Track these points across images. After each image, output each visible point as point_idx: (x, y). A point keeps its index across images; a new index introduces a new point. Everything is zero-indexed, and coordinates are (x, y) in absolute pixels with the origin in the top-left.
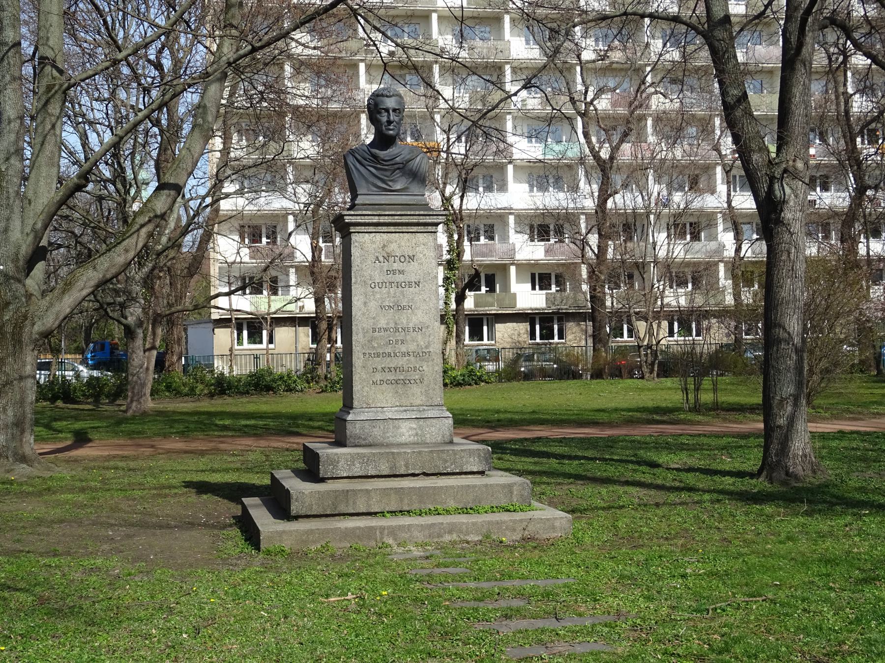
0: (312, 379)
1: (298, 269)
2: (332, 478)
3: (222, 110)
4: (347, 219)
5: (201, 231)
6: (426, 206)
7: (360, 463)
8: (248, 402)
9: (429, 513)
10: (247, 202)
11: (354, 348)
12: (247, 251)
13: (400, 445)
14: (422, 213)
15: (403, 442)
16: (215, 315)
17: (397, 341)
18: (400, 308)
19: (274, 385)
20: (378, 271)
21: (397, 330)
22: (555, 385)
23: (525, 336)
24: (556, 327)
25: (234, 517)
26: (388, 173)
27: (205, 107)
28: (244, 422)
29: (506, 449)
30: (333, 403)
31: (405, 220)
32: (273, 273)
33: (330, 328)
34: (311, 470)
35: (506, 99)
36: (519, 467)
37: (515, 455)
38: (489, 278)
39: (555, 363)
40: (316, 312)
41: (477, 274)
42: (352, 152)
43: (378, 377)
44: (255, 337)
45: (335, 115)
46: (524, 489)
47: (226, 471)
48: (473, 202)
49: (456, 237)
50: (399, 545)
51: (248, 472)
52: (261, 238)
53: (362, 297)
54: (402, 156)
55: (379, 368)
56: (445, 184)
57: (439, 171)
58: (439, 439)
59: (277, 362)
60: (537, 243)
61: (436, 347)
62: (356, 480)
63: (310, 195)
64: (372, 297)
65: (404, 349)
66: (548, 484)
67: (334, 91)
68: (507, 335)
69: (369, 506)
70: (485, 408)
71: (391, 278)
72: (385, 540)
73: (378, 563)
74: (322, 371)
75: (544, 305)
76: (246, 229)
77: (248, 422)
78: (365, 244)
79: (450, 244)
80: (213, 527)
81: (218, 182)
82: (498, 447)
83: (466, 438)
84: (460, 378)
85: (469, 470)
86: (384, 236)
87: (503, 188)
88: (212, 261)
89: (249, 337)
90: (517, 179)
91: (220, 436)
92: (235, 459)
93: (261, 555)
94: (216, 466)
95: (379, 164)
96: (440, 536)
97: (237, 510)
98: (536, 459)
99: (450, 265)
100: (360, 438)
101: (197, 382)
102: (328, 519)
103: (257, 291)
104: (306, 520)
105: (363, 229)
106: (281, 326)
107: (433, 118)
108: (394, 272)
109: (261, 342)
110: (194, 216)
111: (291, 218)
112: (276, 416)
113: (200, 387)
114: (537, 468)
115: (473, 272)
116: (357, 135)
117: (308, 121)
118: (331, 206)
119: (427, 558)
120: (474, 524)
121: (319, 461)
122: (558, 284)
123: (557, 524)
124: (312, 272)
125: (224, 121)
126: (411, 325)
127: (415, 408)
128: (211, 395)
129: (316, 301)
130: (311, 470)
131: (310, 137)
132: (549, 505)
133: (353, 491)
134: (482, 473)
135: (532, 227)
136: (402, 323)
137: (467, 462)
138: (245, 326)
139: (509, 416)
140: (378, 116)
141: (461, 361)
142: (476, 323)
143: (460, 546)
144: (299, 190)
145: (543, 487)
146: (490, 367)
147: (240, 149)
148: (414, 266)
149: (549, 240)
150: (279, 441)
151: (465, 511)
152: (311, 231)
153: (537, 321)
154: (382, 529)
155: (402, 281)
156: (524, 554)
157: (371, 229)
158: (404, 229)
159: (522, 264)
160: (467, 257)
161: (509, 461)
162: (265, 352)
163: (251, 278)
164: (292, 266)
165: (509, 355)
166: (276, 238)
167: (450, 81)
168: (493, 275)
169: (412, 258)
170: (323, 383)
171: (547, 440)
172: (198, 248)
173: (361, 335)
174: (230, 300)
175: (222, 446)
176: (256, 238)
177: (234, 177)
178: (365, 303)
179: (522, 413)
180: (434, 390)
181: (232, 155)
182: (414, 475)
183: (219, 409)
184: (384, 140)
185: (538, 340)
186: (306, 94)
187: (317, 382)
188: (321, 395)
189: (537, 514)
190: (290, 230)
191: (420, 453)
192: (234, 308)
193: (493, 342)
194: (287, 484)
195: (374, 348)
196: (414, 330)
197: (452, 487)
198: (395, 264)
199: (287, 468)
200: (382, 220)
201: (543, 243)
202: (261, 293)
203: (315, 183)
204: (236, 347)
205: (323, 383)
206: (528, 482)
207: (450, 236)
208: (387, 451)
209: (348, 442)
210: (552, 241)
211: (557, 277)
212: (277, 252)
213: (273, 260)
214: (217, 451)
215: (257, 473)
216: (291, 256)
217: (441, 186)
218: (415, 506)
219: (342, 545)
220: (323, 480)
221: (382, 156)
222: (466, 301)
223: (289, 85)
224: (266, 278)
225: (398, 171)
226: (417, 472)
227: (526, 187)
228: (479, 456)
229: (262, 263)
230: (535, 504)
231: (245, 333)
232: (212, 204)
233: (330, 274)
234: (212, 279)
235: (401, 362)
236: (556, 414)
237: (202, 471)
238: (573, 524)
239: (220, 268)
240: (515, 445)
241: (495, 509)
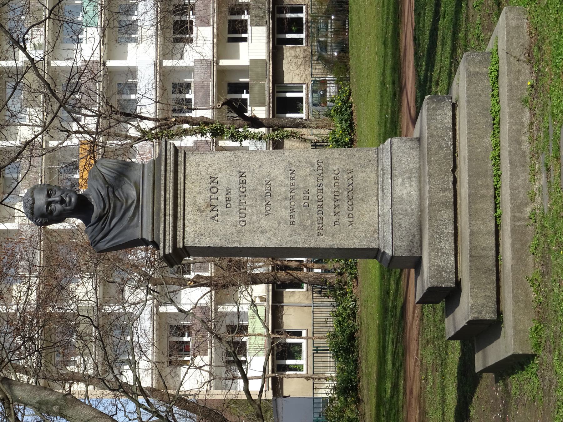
0: (342, 289)
1: (218, 302)
2: (456, 273)
3: (42, 382)
4: (169, 250)
5: (175, 409)
6: (156, 163)
7: (440, 242)
8: (367, 360)
9: (497, 166)
10: (144, 358)
11: (311, 246)
12: (198, 358)
13: (421, 197)
14: (163, 167)
15: (417, 193)
16: (269, 395)
17: (305, 198)
18: (268, 194)
19: (348, 331)
21: (293, 198)
22: (355, 18)
23: (298, 50)
24: (289, 15)
25: (497, 382)
26: (119, 204)
27: (40, 403)
28: (389, 366)
29: (426, 76)
30: (370, 269)
31: (170, 187)
32: (223, 330)
33: (285, 268)
34: (446, 296)
35: (36, 69)
36: (447, 62)
37: (433, 66)
38: (232, 89)
39: (330, 18)
40: (268, 283)
41: (228, 103)
42: (94, 243)
43: (344, 220)
44: (293, 351)
45: (48, 258)
46: (473, 60)
47: (443, 388)
48: (147, 106)
49: (186, 126)
50: (533, 200)
51: (446, 364)
52: (184, 343)
53: (255, 236)
54: (100, 188)
55: (334, 218)
56: (127, 137)
57: (112, 143)
58: (415, 153)
59: (322, 327)
60: (194, 36)
61: (314, 155)
62: (459, 246)
63: (137, 287)
64: (256, 225)
65: (314, 191)
66: (467, 31)
67: (22, 258)
68: (297, 71)
69: (488, 233)
70: (378, 98)
72: (526, 216)
73: (553, 225)
74: (333, 278)
75: (264, 28)
76: (174, 358)
77: (389, 362)
78: (197, 230)
79: (194, 133)
80: (506, 405)
81: (121, 388)
82: (424, 87)
83: (414, 122)
84: (344, 124)
85: (450, 121)
86: (188, 209)
87: (132, 72)
88: (208, 397)
89: (293, 358)
90: (124, 56)
91: (405, 394)
92: (430, 378)
93: (541, 353)
94: (438, 399)
95: (106, 214)
96: (523, 155)
97: (488, 378)
98: (439, 43)
99: (218, 133)
100: (412, 241)
101: (343, 417)
102: (501, 278)
103: (242, 348)
104: (502, 303)
105: (180, 234)
106: (282, 323)
107: (54, 149)
109: (300, 345)
110: (159, 416)
111: (162, 309)
112: (383, 331)
113: (348, 413)
114: (449, 42)
115: (225, 107)
116: (72, 233)
117: (54, 288)
118: (151, 265)
119: (548, 170)
120: (511, 116)
121: (437, 288)
122: (241, 13)
123: (513, 23)
124: (222, 287)
125: (55, 380)
126: (288, 182)
127: (380, 179)
128: (358, 401)
129: (255, 283)
130: (446, 296)
131: (72, 286)
132: (492, 30)
133: (471, 250)
134: (454, 106)
135: (177, 40)
136: (285, 191)
137: (442, 122)
138: (281, 362)
139: (388, 71)
140: (55, 214)
141: (326, 122)
142: (283, 104)
143: (535, 132)
144: (132, 299)
145: (470, 36)
146: (333, 90)
147: (84, 363)
148: (222, 178)
149: (191, 22)
150: (411, 328)
151: (496, 126)
152: (177, 287)
153: (282, 36)
154: (514, 219)
155: (240, 189)
156: (546, 62)
157: (180, 224)
158: (180, 187)
159: (217, 52)
160: (208, 114)
161: (439, 74)
162: (310, 341)
163: (228, 354)
164: (216, 309)
165: (319, 68)
166: (184, 326)
167: (12, 128)
168: (230, 85)
169: (213, 180)
170: (347, 277)
171: (417, 29)
172: (194, 413)
173: (298, 238)
174: (252, 378)
175: (416, 391)
176: (184, 348)
177: (116, 371)
178: (262, 232)
179: (385, 56)
180: (360, 158)
181: (91, 372)
182: (455, 182)
183: (373, 393)
184: (82, 207)
185: (303, 36)
186: (25, 289)
187: (346, 284)
188: (360, 279)
189: (502, 46)
190: (176, 310)
191: (430, 175)
192: (261, 374)
193: (304, 86)
194: (461, 323)
195: (312, 224)
196: (294, 179)
197: (470, 139)
199: (442, 321)
200: (170, 211)
201: (195, 29)
202: (245, 343)
203: (125, 282)
204: (304, 372)
205: (347, 277)
206: (465, 55)
207: (186, 132)
208: (427, 211)
209: (416, 255)
210: (192, 17)
211: (232, 13)
212: (200, 325)
213: (209, 329)
214: (421, 398)
215: (447, 354)
216: (204, 309)
217: (129, 141)
218: (490, 181)
219: (531, 264)
220: (458, 283)
221: (100, 210)
222: (258, 116)
223: (14, 308)
224: (229, 338)
225: (116, 194)
226: (451, 179)
227: (131, 46)
228: (435, 109)
229: (212, 345)
230: (490, 47)
231: (289, 362)
232: (146, 396)
233: (225, 267)
234: (230, 397)
235: (328, 193)
236: (388, 19)
237: (443, 414)
238: (514, 5)
239: (216, 389)
240: (422, 66)
241: (495, 92)
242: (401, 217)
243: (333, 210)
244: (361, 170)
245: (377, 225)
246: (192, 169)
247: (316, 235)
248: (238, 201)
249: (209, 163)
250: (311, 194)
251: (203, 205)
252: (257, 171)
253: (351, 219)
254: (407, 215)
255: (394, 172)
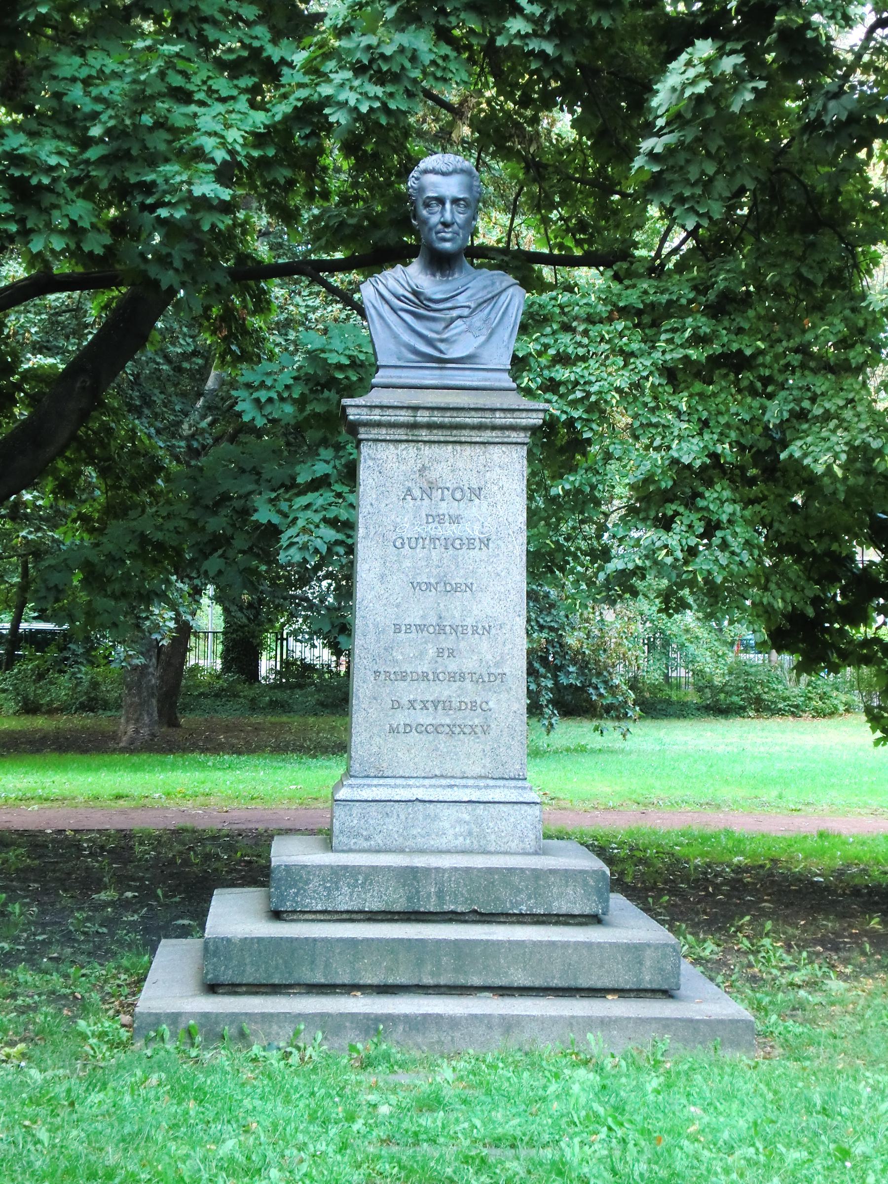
7: (349, 885)
20: (410, 516)
26: (440, 326)
65: (453, 666)
71: (433, 529)
105: (383, 433)
108: (440, 519)
126: (469, 621)
127: (471, 782)
169: (477, 493)
173: (372, 637)
178: (382, 576)
180: (509, 748)
197: (520, 944)
198: (444, 505)
228: (585, 884)
242: (403, 817)
243: (419, 698)
244: (487, 748)
245: (390, 774)
246: (495, 457)
247: (376, 668)
248: (439, 534)
249: (506, 486)
250: (447, 662)
251: (433, 475)
252: (490, 568)
253: (401, 729)
254: (405, 828)
255: (482, 806)
